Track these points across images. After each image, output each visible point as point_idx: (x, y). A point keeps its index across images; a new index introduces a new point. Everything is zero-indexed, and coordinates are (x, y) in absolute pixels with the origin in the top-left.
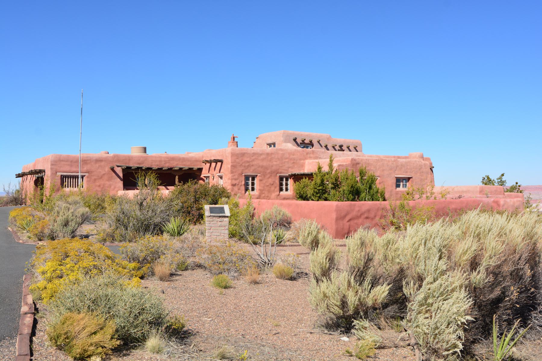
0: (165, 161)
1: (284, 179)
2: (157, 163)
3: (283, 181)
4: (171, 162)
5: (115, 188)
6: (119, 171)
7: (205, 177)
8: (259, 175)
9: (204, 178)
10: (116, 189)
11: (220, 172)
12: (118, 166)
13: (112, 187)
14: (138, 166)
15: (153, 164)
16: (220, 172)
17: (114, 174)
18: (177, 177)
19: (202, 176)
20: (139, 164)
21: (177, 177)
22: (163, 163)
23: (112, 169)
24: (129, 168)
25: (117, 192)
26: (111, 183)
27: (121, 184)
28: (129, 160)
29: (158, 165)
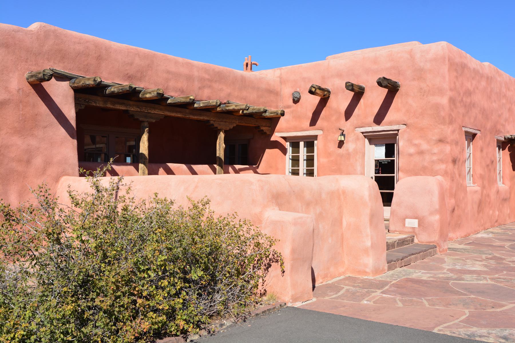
0: (202, 80)
1: (302, 144)
2: (182, 84)
3: (298, 147)
4: (216, 85)
5: (47, 163)
6: (62, 93)
7: (285, 138)
8: (479, 133)
9: (282, 141)
10: (52, 171)
11: (313, 122)
12: (61, 77)
13: (38, 161)
14: (126, 84)
15: (172, 84)
16: (313, 122)
17: (43, 108)
18: (222, 135)
19: (276, 136)
20: (130, 77)
21: (222, 135)
22: (197, 84)
23: (37, 85)
24: (98, 89)
25: (57, 180)
26: (33, 142)
27: (68, 149)
28: (99, 58)
29: (182, 91)
